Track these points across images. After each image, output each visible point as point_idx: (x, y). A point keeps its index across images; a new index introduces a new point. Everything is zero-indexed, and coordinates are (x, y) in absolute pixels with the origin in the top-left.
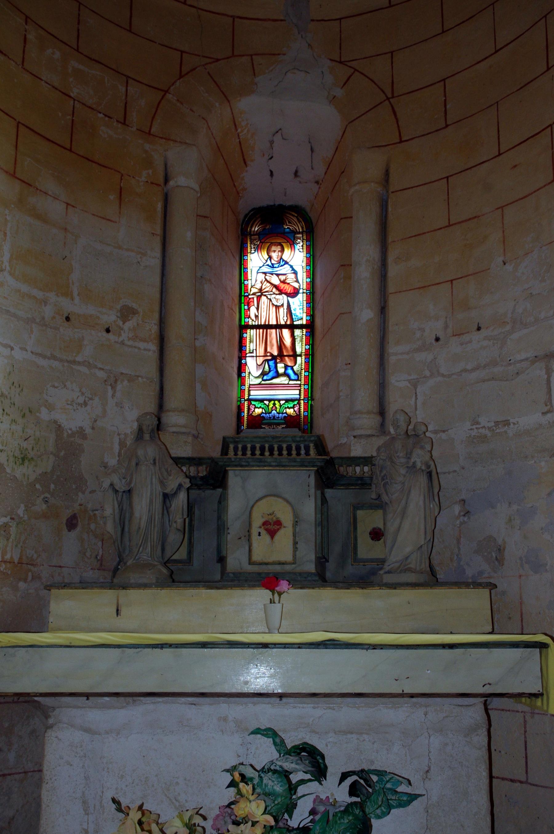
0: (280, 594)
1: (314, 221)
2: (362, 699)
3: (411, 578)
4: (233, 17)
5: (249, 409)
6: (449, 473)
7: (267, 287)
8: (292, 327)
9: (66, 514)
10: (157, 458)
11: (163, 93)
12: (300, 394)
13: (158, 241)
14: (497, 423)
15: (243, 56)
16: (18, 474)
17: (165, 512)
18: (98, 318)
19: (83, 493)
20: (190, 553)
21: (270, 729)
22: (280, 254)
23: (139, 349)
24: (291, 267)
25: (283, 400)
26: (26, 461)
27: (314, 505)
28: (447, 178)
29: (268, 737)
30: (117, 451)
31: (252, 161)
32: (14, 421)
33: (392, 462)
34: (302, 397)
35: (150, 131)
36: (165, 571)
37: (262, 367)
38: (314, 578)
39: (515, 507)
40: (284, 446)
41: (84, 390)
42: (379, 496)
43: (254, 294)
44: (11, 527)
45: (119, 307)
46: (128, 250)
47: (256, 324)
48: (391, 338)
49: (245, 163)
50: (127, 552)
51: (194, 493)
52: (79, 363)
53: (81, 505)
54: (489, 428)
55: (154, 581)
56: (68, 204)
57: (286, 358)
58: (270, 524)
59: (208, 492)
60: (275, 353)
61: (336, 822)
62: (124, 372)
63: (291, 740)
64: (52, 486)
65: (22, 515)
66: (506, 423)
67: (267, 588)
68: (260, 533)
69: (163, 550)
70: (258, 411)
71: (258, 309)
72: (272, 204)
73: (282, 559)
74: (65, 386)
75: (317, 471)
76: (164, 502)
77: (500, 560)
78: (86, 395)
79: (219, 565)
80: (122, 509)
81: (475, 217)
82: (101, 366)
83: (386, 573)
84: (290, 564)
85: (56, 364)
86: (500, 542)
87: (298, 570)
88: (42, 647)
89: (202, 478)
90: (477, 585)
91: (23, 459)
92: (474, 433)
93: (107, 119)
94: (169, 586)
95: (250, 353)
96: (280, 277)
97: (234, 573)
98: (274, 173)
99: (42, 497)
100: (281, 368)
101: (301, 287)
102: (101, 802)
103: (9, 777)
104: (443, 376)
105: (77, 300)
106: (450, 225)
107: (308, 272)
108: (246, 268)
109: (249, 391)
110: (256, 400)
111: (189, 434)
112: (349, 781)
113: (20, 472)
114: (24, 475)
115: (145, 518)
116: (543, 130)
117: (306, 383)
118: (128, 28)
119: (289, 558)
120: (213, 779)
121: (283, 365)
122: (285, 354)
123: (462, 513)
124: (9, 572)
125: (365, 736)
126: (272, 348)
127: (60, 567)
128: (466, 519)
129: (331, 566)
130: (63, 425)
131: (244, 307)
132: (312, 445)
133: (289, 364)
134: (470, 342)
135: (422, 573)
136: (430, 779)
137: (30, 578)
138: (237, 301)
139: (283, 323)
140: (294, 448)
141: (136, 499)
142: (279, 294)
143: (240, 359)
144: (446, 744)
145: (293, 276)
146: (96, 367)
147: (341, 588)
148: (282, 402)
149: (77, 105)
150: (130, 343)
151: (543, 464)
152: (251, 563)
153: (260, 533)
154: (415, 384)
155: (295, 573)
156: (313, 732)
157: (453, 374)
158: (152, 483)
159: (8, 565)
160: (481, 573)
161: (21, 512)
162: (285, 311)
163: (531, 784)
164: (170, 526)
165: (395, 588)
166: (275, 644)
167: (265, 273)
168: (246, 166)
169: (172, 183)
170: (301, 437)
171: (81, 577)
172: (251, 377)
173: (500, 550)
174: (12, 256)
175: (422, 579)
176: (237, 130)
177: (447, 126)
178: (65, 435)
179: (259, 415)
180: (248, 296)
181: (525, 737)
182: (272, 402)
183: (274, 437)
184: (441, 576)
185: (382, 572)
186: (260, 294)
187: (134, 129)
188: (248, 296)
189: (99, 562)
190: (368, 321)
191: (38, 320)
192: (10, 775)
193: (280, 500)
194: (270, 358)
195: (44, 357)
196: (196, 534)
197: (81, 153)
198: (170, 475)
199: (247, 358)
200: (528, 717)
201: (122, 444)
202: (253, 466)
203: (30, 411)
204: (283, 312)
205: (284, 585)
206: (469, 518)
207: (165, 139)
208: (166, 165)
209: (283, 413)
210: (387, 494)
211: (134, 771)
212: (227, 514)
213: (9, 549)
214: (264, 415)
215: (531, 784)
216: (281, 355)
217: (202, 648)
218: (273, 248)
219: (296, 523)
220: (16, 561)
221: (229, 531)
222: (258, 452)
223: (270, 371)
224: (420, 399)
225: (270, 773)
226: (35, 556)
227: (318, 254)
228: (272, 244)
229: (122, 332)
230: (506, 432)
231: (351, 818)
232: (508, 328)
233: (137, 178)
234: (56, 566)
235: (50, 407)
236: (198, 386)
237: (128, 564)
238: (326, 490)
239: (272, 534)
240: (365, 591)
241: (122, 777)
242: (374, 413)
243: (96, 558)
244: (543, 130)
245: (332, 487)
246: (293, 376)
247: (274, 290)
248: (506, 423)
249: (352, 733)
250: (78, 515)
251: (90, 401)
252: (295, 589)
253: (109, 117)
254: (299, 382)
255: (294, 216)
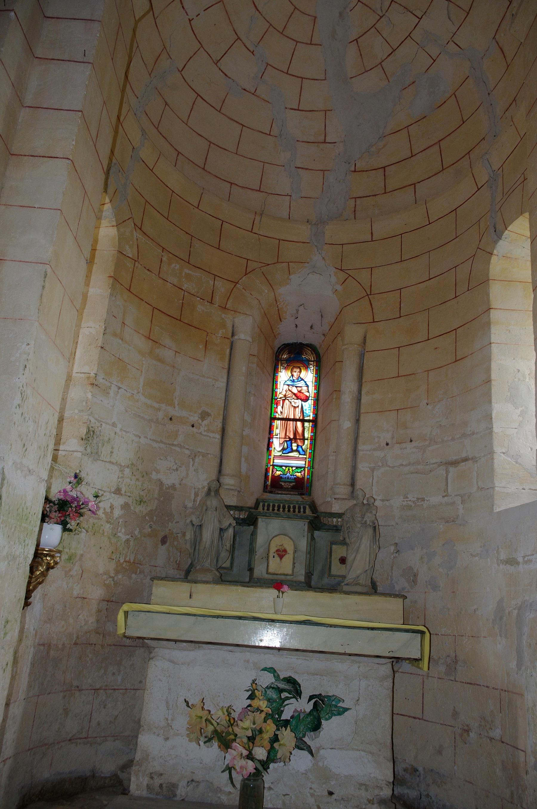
0: (283, 593)
1: (321, 355)
2: (323, 655)
3: (359, 589)
4: (279, 240)
5: (273, 471)
6: (389, 526)
7: (289, 394)
8: (303, 421)
9: (162, 534)
10: (218, 507)
11: (235, 284)
12: (305, 464)
13: (226, 371)
14: (418, 499)
15: (284, 262)
16: (137, 510)
17: (220, 539)
18: (188, 418)
19: (172, 523)
20: (232, 564)
21: (272, 668)
22: (299, 373)
23: (210, 437)
24: (305, 382)
25: (294, 467)
26: (142, 503)
27: (306, 542)
28: (399, 347)
29: (271, 673)
30: (193, 499)
31: (285, 319)
32: (138, 479)
33: (353, 519)
34: (307, 466)
35: (226, 306)
36: (218, 574)
37: (283, 445)
38: (303, 585)
39: (425, 551)
40: (292, 506)
41: (177, 462)
42: (345, 539)
43: (280, 398)
44: (131, 541)
45: (200, 412)
46: (208, 378)
47: (281, 417)
48: (361, 440)
49: (281, 320)
50: (196, 561)
51: (238, 527)
52: (175, 445)
53: (170, 530)
54: (413, 502)
55: (211, 580)
56: (176, 352)
57: (298, 440)
58: (280, 551)
59: (245, 528)
60: (292, 437)
61: (304, 720)
62: (200, 451)
63: (283, 675)
64: (155, 518)
65: (137, 535)
66: (423, 500)
67: (276, 589)
68: (274, 556)
69: (217, 561)
70: (278, 473)
71: (282, 408)
72: (296, 342)
73: (286, 573)
74: (167, 459)
75: (310, 522)
76: (220, 533)
77: (415, 582)
78: (178, 464)
79: (249, 572)
80: (196, 535)
81: (413, 374)
82: (188, 447)
83: (345, 585)
84: (290, 575)
85: (162, 445)
86: (415, 570)
87: (295, 579)
88: (154, 612)
89: (242, 519)
90: (396, 596)
91: (141, 502)
92: (405, 503)
93: (202, 300)
94: (220, 584)
95: (276, 435)
96: (298, 388)
97: (257, 579)
98: (298, 326)
99: (149, 524)
100: (294, 447)
101: (311, 396)
102: (176, 704)
103: (117, 691)
104: (389, 466)
105: (177, 408)
106: (398, 377)
107: (315, 386)
108: (277, 381)
109: (274, 460)
110: (277, 466)
111: (236, 490)
112: (314, 700)
113: (138, 509)
114: (140, 511)
115: (208, 543)
116: (452, 331)
117: (310, 457)
118: (218, 247)
119: (290, 572)
120: (239, 695)
121: (296, 445)
122: (298, 438)
123: (395, 551)
124: (128, 568)
125: (325, 677)
126: (289, 433)
127: (155, 566)
128: (397, 555)
129: (315, 578)
130: (163, 482)
131: (274, 406)
132: (307, 507)
133: (300, 444)
134: (406, 448)
135: (366, 586)
136: (359, 705)
137: (138, 572)
138: (270, 402)
139: (298, 418)
140: (297, 508)
141: (204, 530)
142: (297, 399)
143: (269, 439)
144: (369, 685)
145: (306, 388)
146: (184, 447)
147: (318, 592)
148: (294, 468)
149: (186, 294)
150: (205, 433)
151: (441, 526)
152: (268, 573)
153: (274, 556)
154: (373, 470)
155: (292, 581)
156: (296, 672)
157: (395, 467)
158: (214, 522)
159: (128, 564)
160: (403, 589)
161: (137, 532)
162: (300, 410)
163: (425, 720)
164: (222, 548)
165: (349, 594)
166: (278, 620)
167: (288, 385)
168: (281, 322)
169: (236, 337)
170: (301, 502)
171: (167, 573)
172: (275, 451)
173: (415, 576)
174: (144, 384)
175: (365, 590)
176: (277, 303)
177: (400, 317)
178: (164, 488)
179: (279, 476)
180: (277, 399)
181: (423, 691)
182: (288, 468)
183: (286, 501)
184: (380, 589)
185: (343, 584)
186: (284, 398)
187: (217, 306)
188: (277, 399)
189: (178, 565)
190: (347, 428)
191: (155, 420)
192: (118, 689)
193: (286, 537)
194: (288, 439)
195: (156, 442)
196: (236, 552)
197: (186, 322)
198: (225, 518)
199: (274, 439)
200: (425, 680)
201: (196, 495)
202: (273, 517)
203: (147, 474)
204: (298, 410)
205: (285, 588)
206: (399, 554)
207: (234, 311)
208: (233, 326)
209: (294, 476)
210: (349, 538)
211: (196, 687)
212: (256, 543)
213: (128, 554)
214: (282, 476)
215: (425, 720)
216: (295, 438)
217: (239, 619)
218: (295, 370)
219: (295, 552)
220: (132, 561)
221: (256, 554)
222: (276, 508)
223: (287, 448)
224: (375, 479)
225: (271, 689)
226: (142, 559)
227: (322, 377)
228: (294, 367)
229: (201, 427)
230: (422, 505)
231: (311, 717)
232: (427, 443)
233: (216, 335)
234: (153, 566)
235: (158, 472)
236: (243, 459)
237: (197, 568)
238: (315, 531)
239: (281, 557)
240: (331, 594)
241: (189, 690)
242: (347, 485)
243: (176, 562)
244: (452, 331)
245: (319, 530)
246: (301, 452)
247: (294, 396)
248: (423, 500)
249: (317, 675)
250: (168, 536)
251: (180, 468)
252: (292, 590)
253: (203, 299)
254: (305, 456)
255: (309, 350)
